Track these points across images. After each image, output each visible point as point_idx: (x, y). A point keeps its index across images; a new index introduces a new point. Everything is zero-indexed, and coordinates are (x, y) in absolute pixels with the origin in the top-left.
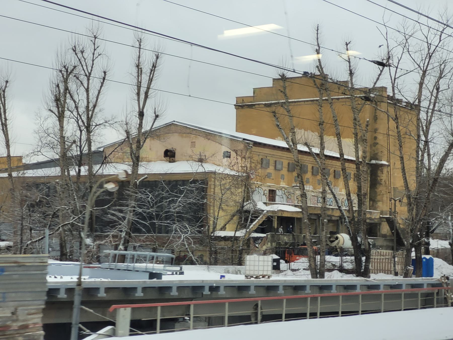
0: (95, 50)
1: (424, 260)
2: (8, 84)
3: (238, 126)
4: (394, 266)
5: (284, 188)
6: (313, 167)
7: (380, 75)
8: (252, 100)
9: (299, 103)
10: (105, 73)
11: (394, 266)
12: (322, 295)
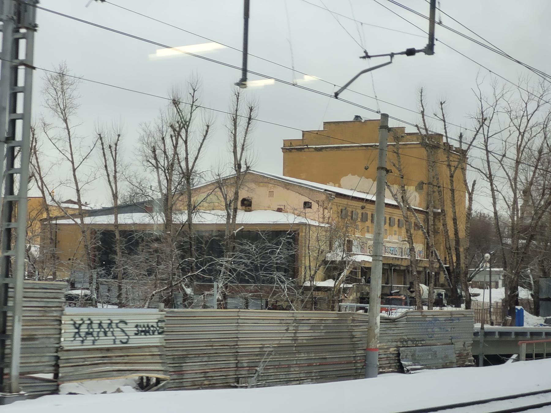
0: (193, 102)
1: (516, 311)
2: (120, 138)
3: (286, 169)
4: (490, 317)
5: (358, 237)
6: (399, 220)
7: (476, 135)
8: (301, 144)
9: (352, 148)
10: (208, 126)
11: (490, 317)
12: (548, 340)
